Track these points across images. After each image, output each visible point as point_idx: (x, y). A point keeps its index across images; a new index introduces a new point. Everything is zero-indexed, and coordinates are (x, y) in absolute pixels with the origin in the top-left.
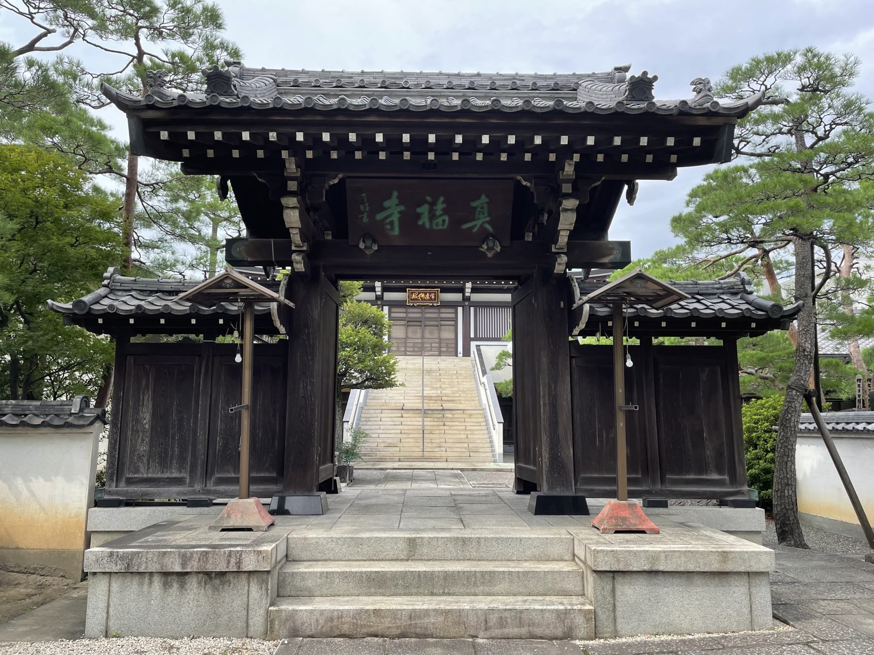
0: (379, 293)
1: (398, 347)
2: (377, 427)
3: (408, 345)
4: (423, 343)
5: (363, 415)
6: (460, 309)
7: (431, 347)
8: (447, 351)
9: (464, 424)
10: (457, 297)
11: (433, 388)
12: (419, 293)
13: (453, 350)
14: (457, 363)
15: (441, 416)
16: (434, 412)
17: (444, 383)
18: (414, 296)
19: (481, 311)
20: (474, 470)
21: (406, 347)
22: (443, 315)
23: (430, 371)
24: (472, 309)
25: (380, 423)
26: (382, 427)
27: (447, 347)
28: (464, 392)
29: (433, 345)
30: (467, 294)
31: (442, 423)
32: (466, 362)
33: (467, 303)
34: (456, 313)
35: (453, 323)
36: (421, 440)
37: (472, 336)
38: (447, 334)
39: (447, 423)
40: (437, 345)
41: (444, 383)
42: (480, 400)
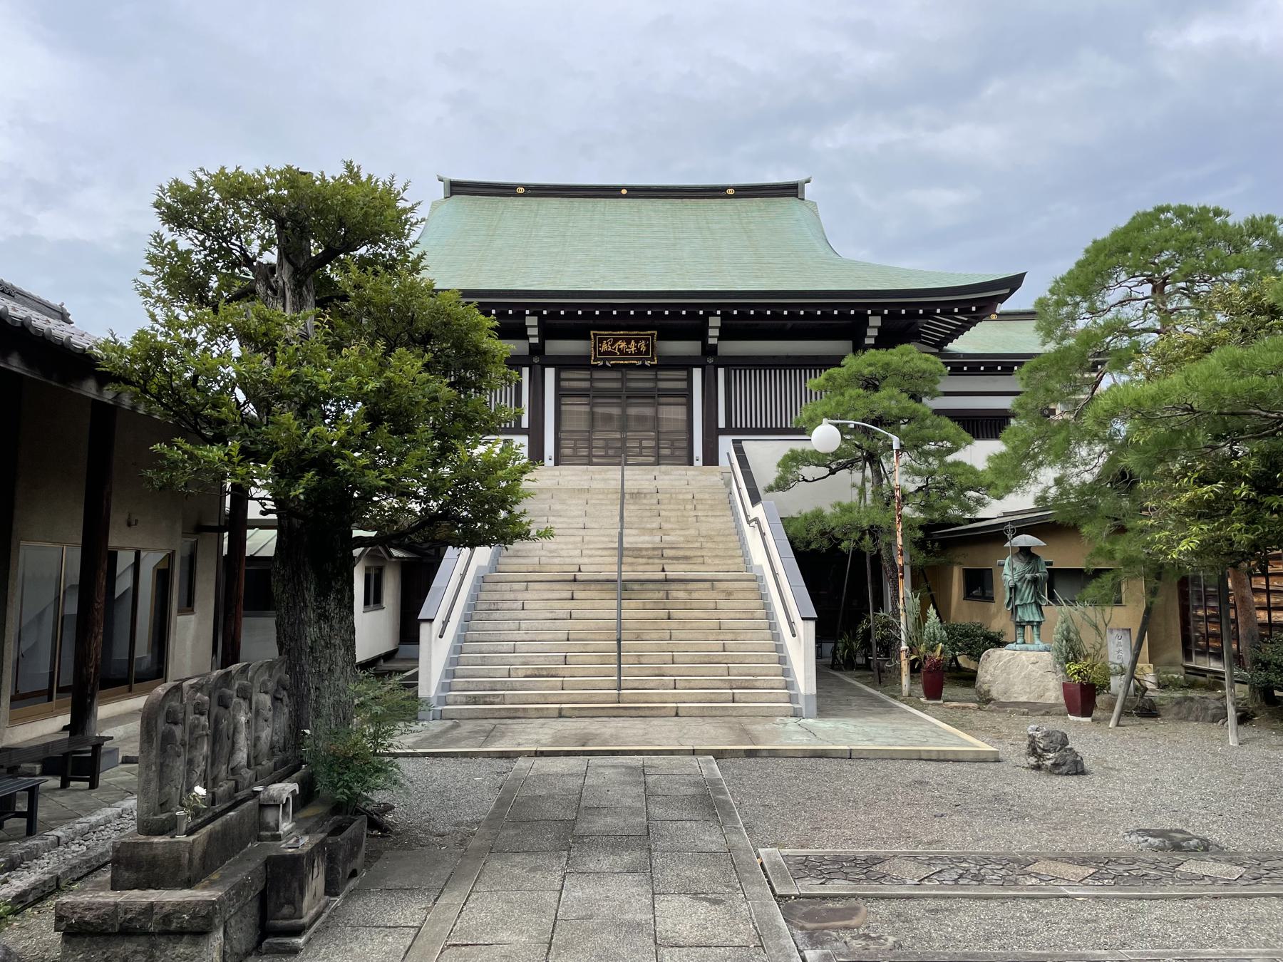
0: (536, 340)
1: (575, 448)
2: (513, 625)
3: (595, 443)
4: (623, 440)
5: (483, 596)
6: (697, 374)
7: (641, 448)
8: (672, 456)
9: (715, 614)
10: (689, 348)
11: (644, 531)
12: (616, 341)
13: (684, 453)
14: (696, 477)
15: (662, 594)
16: (649, 584)
17: (667, 520)
18: (605, 347)
19: (737, 374)
20: (751, 754)
21: (590, 448)
22: (663, 385)
23: (637, 495)
24: (721, 371)
25: (522, 614)
26: (524, 624)
27: (672, 447)
28: (709, 538)
29: (645, 443)
30: (712, 341)
31: (663, 613)
32: (712, 476)
33: (710, 361)
34: (690, 380)
35: (683, 400)
36: (614, 660)
37: (722, 424)
38: (672, 413)
39: (674, 613)
40: (652, 443)
41: (667, 520)
42: (746, 555)
